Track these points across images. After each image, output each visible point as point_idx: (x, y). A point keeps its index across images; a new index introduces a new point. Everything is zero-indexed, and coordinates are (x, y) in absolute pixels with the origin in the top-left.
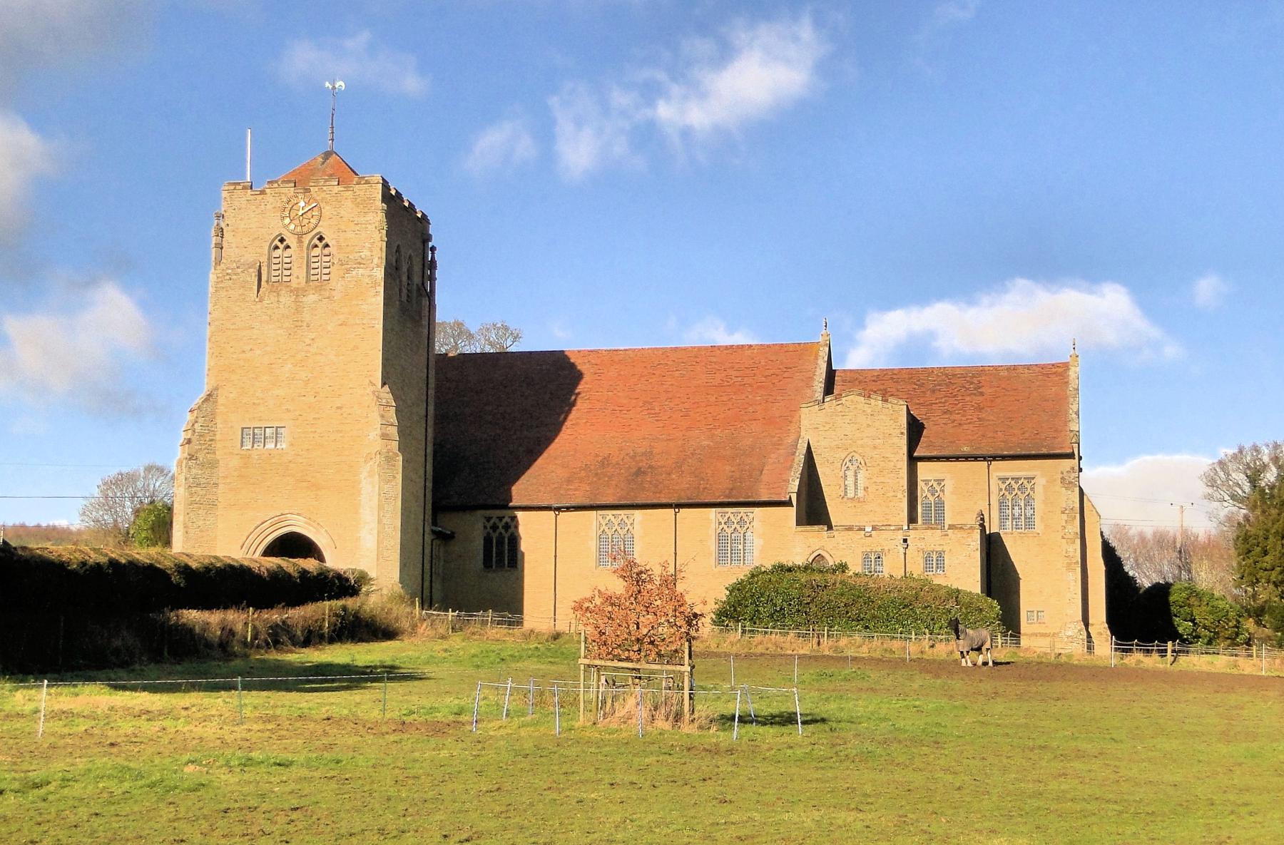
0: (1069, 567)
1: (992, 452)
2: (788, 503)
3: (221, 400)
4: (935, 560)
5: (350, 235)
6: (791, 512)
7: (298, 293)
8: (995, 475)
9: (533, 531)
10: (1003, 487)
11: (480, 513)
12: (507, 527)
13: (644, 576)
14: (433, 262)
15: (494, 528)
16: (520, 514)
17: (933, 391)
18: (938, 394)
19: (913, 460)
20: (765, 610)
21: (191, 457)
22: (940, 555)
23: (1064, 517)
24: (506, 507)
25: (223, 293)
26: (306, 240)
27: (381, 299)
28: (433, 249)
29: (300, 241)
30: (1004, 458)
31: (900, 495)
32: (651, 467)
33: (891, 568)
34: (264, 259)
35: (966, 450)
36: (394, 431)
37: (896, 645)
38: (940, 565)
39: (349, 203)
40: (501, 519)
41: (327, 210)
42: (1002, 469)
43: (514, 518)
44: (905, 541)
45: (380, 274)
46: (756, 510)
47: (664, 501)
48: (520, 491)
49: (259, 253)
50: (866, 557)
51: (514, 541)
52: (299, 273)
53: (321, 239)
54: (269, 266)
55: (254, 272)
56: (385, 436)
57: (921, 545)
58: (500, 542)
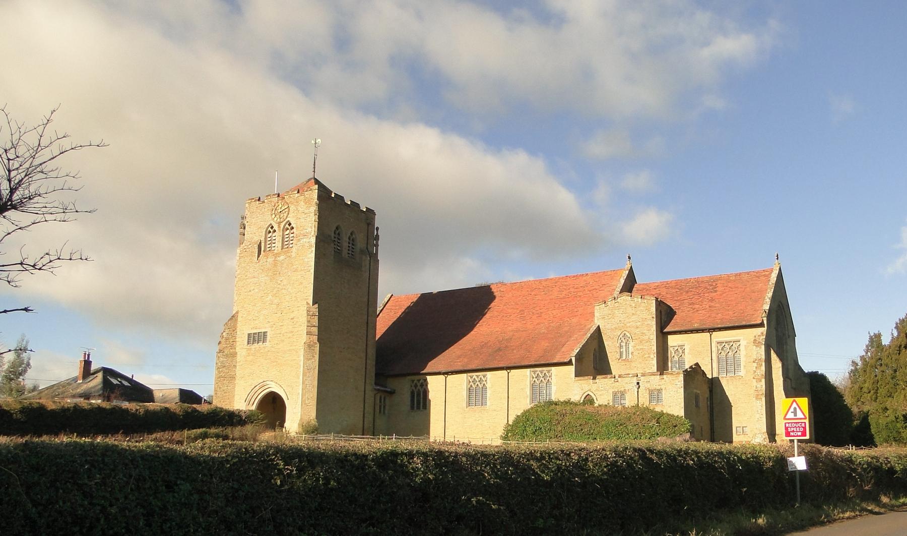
0: (757, 397)
1: (712, 326)
2: (569, 363)
3: (239, 319)
4: (655, 394)
5: (302, 220)
6: (571, 369)
7: (277, 255)
8: (714, 340)
9: (434, 384)
10: (720, 348)
11: (409, 377)
12: (422, 385)
13: (890, 425)
14: (377, 236)
15: (416, 386)
16: (428, 377)
17: (687, 292)
18: (690, 294)
19: (662, 335)
20: (530, 430)
21: (220, 351)
22: (660, 391)
23: (755, 365)
24: (419, 374)
25: (242, 259)
26: (282, 226)
27: (313, 255)
28: (377, 229)
29: (279, 227)
30: (720, 329)
31: (652, 356)
32: (506, 347)
33: (629, 401)
34: (263, 239)
35: (696, 326)
36: (315, 330)
37: (342, 444)
38: (659, 399)
39: (302, 203)
40: (419, 380)
41: (292, 208)
42: (718, 336)
43: (426, 380)
44: (638, 383)
45: (313, 240)
46: (553, 368)
47: (500, 366)
48: (431, 366)
49: (260, 236)
50: (615, 394)
51: (426, 393)
52: (278, 244)
53: (290, 224)
54: (265, 242)
55: (256, 247)
56: (309, 333)
57: (648, 385)
58: (419, 395)
